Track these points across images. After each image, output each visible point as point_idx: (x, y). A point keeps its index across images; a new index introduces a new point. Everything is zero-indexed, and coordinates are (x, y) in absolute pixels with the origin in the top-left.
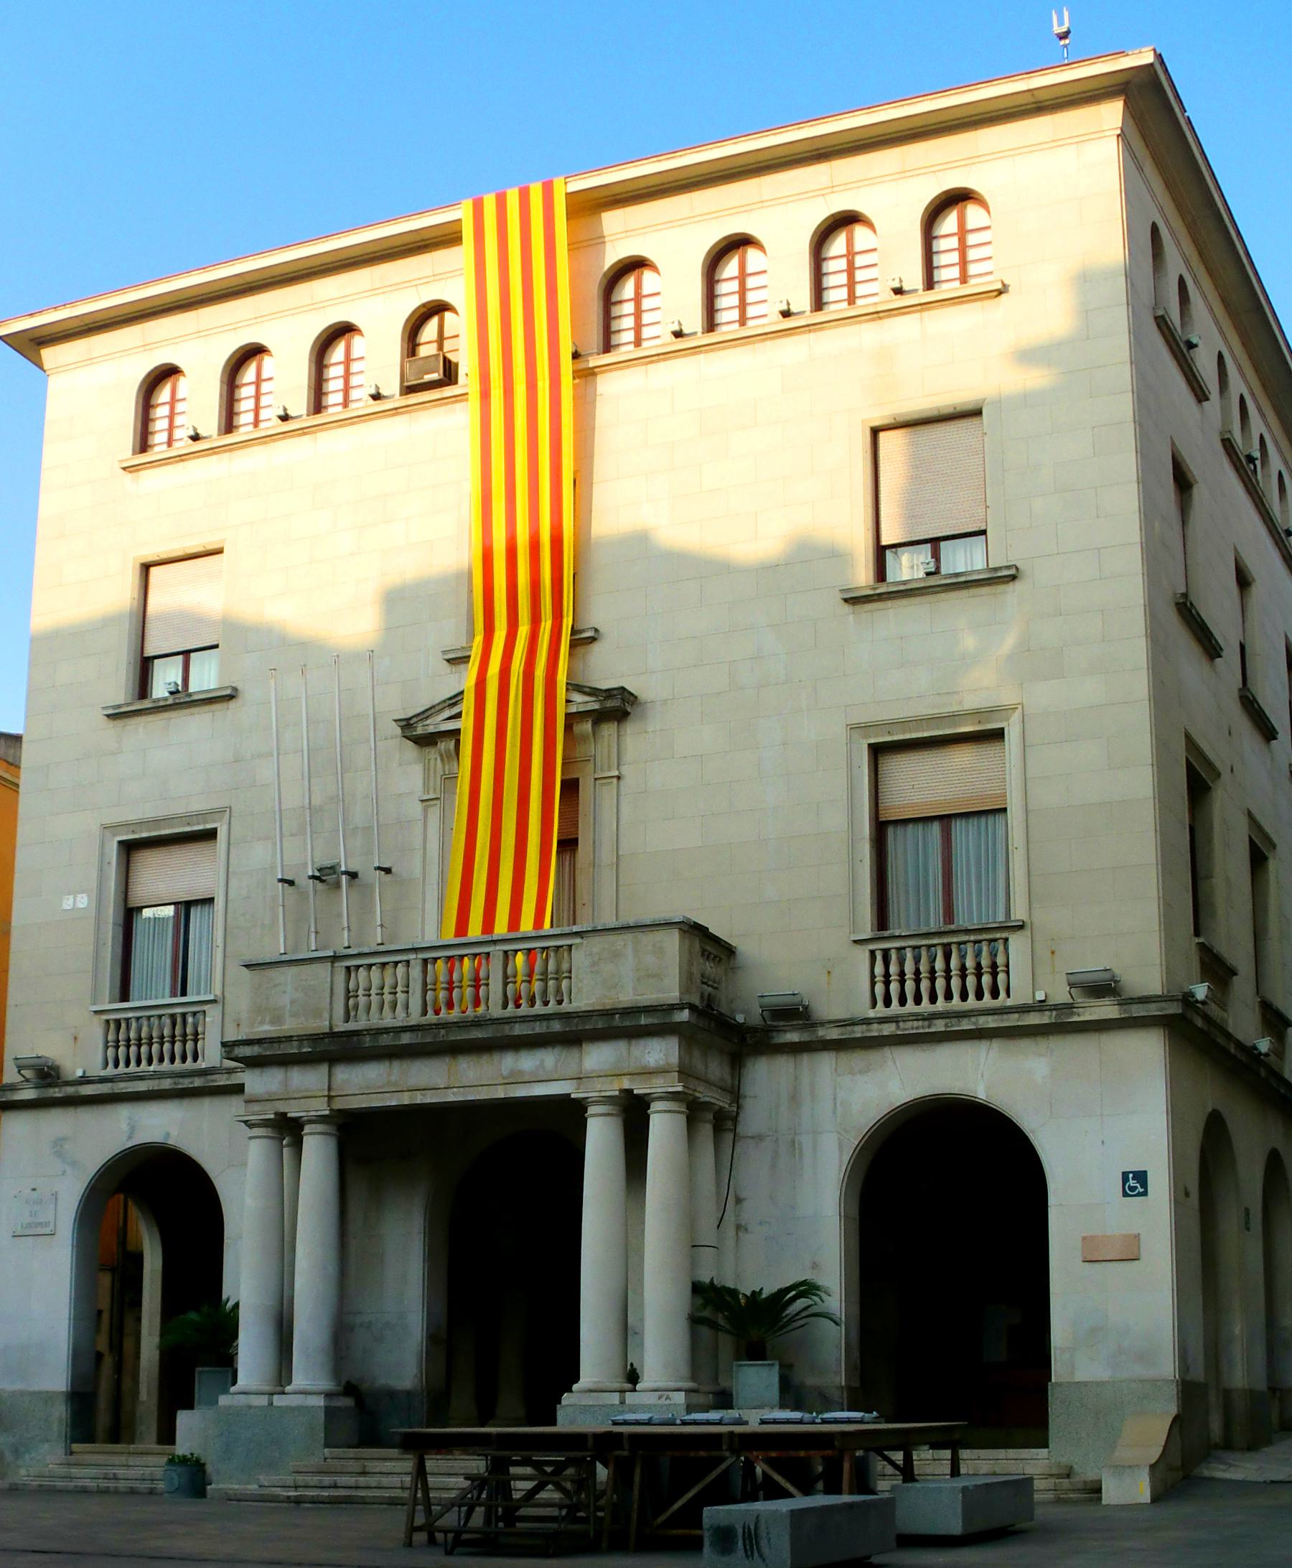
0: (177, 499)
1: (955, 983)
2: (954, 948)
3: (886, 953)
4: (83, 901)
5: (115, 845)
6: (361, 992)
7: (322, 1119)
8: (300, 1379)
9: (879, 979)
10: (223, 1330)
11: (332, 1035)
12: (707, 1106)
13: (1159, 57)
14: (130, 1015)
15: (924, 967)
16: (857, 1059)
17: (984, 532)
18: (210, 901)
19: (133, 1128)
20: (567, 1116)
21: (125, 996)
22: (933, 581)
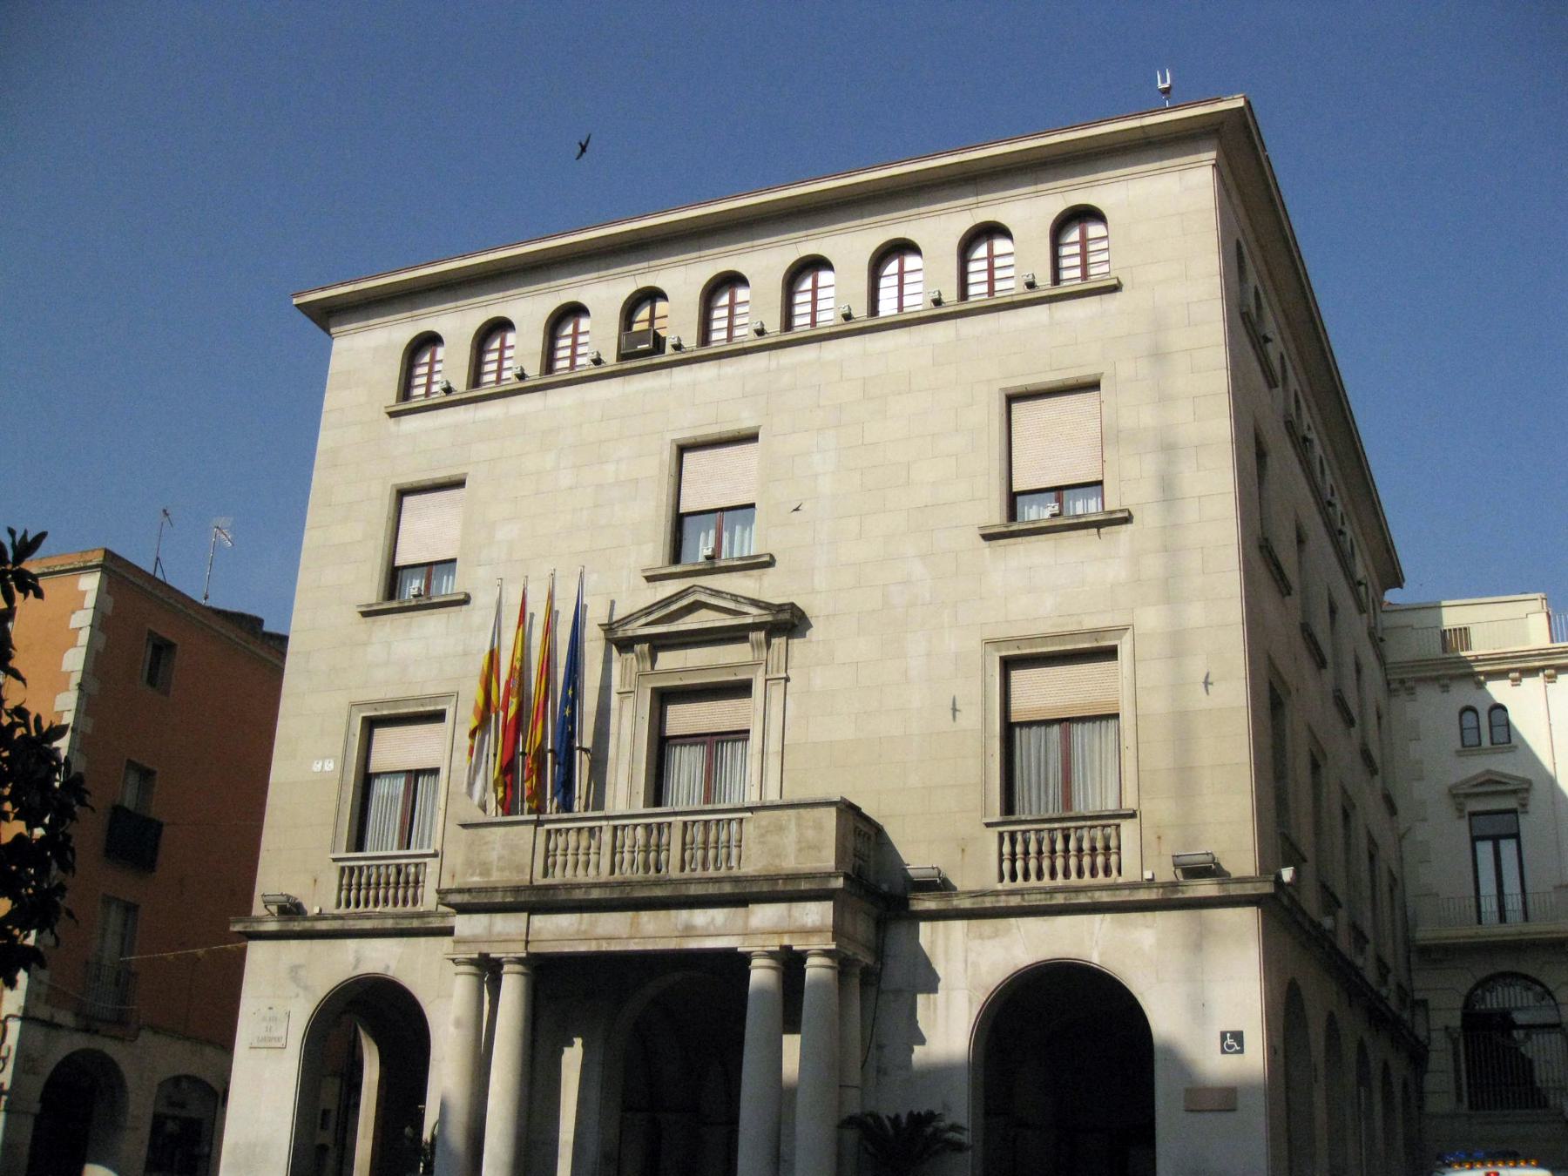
0: (429, 441)
2: (1072, 832)
3: (1013, 835)
4: (330, 766)
5: (649, 692)
6: (559, 852)
7: (519, 961)
9: (1006, 856)
11: (532, 887)
13: (1248, 102)
14: (362, 863)
16: (987, 925)
17: (1100, 483)
18: (434, 772)
22: (1059, 521)
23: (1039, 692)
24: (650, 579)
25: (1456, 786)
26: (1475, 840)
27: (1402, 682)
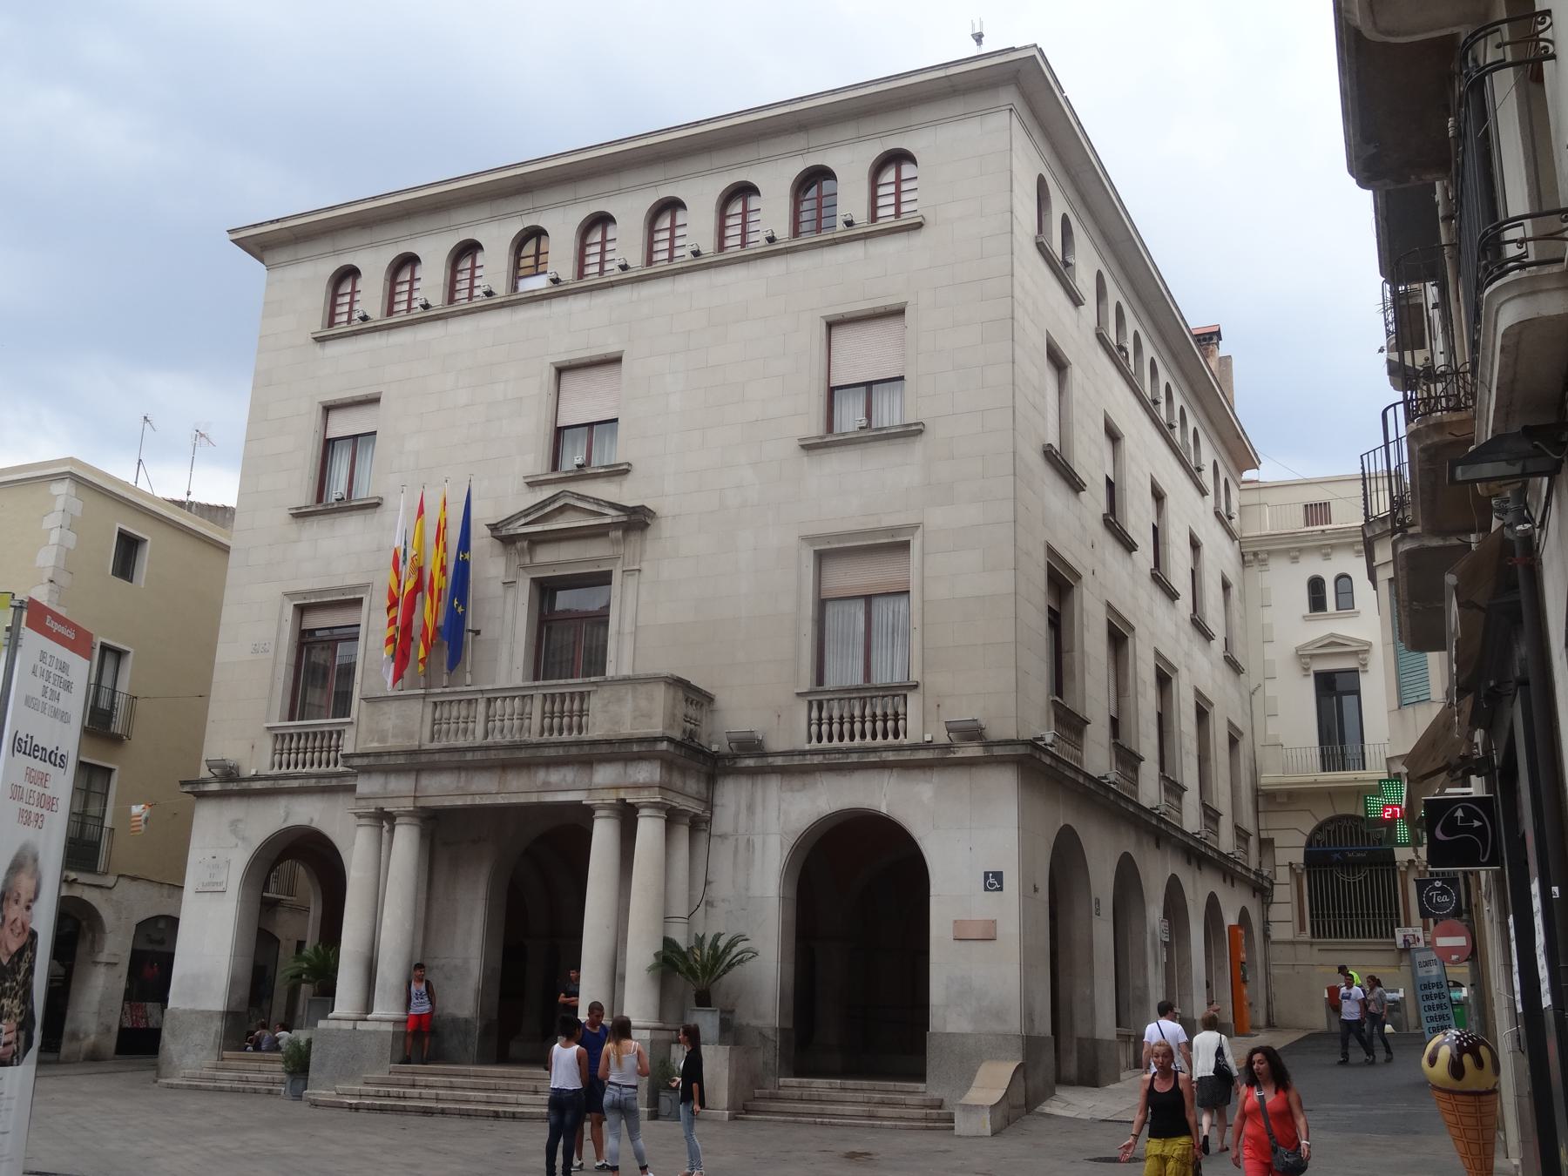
8: (377, 1012)
11: (418, 752)
12: (683, 813)
16: (796, 782)
23: (849, 577)
24: (531, 485)
27: (1255, 554)
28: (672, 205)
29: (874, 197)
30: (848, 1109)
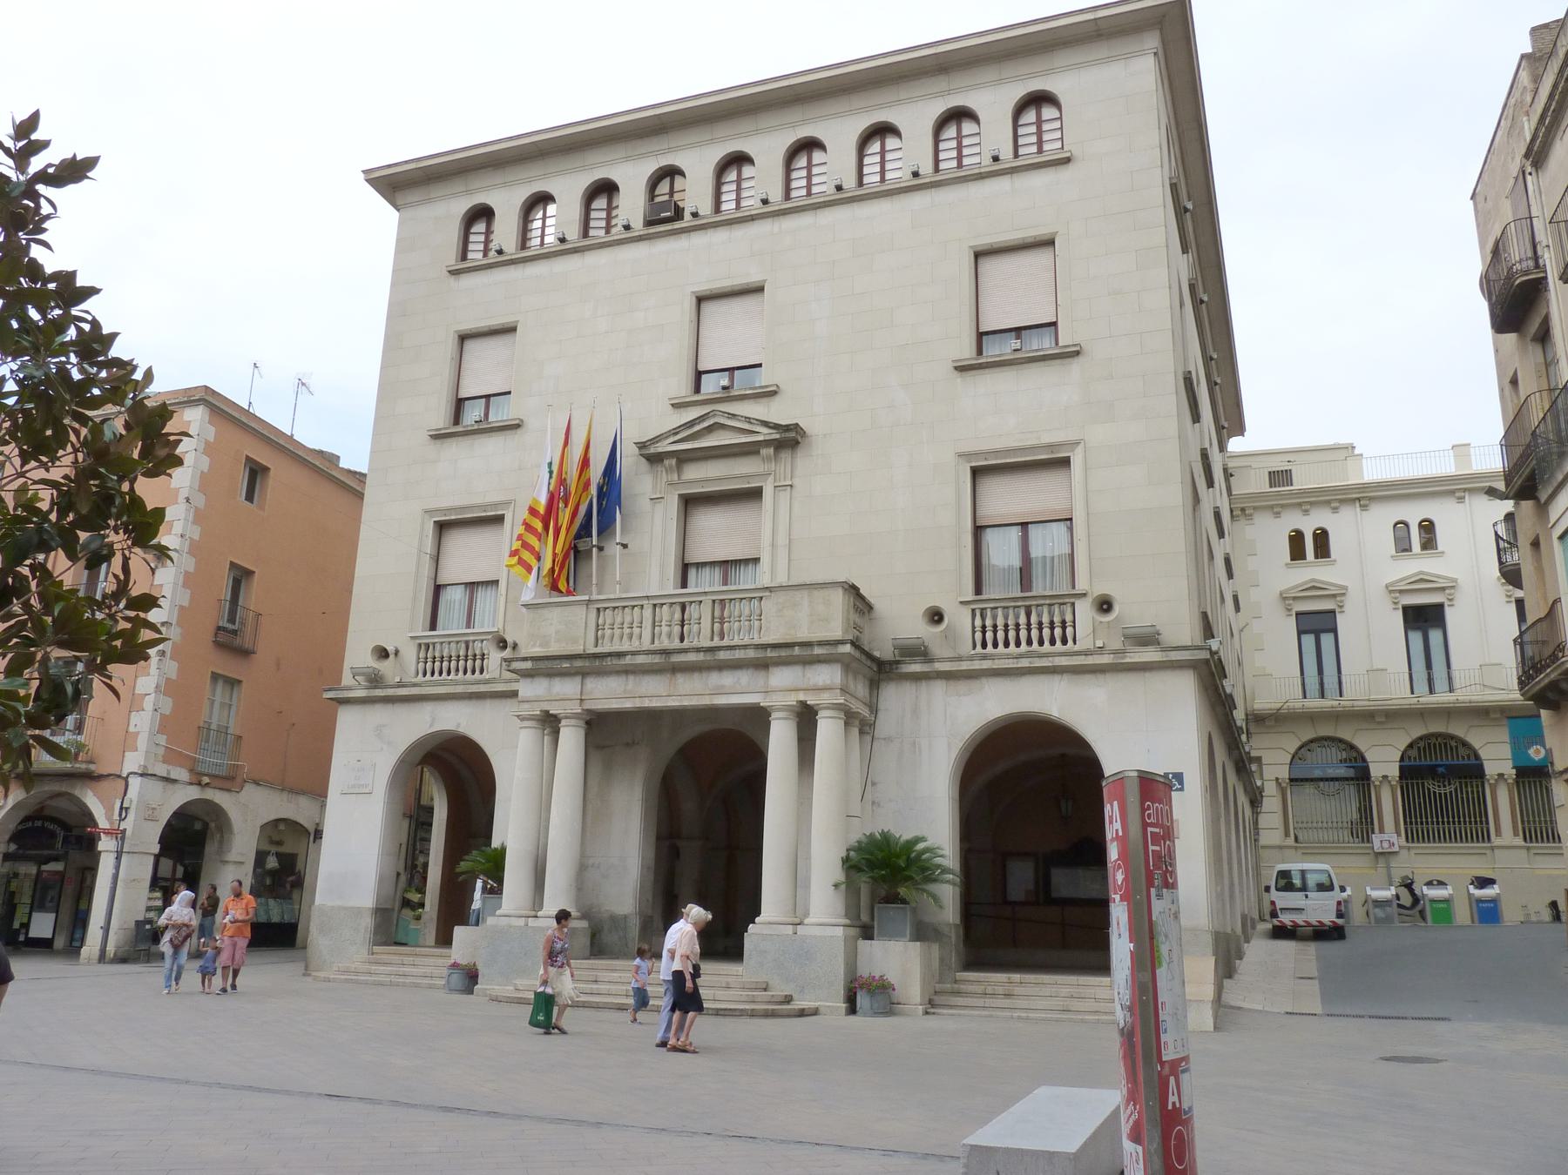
1: (1035, 633)
7: (575, 716)
10: (495, 867)
15: (989, 622)
16: (962, 686)
19: (433, 720)
20: (759, 716)
21: (433, 627)
25: (1287, 590)
26: (1300, 633)
27: (1243, 510)
28: (810, 145)
29: (788, 180)
30: (1041, 1004)
